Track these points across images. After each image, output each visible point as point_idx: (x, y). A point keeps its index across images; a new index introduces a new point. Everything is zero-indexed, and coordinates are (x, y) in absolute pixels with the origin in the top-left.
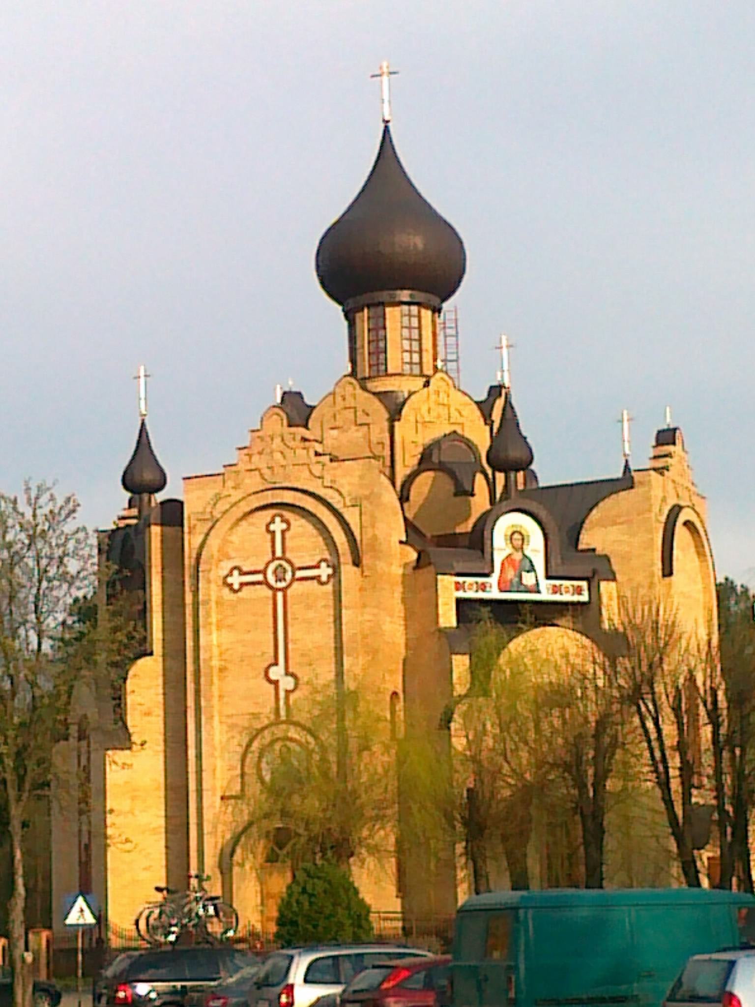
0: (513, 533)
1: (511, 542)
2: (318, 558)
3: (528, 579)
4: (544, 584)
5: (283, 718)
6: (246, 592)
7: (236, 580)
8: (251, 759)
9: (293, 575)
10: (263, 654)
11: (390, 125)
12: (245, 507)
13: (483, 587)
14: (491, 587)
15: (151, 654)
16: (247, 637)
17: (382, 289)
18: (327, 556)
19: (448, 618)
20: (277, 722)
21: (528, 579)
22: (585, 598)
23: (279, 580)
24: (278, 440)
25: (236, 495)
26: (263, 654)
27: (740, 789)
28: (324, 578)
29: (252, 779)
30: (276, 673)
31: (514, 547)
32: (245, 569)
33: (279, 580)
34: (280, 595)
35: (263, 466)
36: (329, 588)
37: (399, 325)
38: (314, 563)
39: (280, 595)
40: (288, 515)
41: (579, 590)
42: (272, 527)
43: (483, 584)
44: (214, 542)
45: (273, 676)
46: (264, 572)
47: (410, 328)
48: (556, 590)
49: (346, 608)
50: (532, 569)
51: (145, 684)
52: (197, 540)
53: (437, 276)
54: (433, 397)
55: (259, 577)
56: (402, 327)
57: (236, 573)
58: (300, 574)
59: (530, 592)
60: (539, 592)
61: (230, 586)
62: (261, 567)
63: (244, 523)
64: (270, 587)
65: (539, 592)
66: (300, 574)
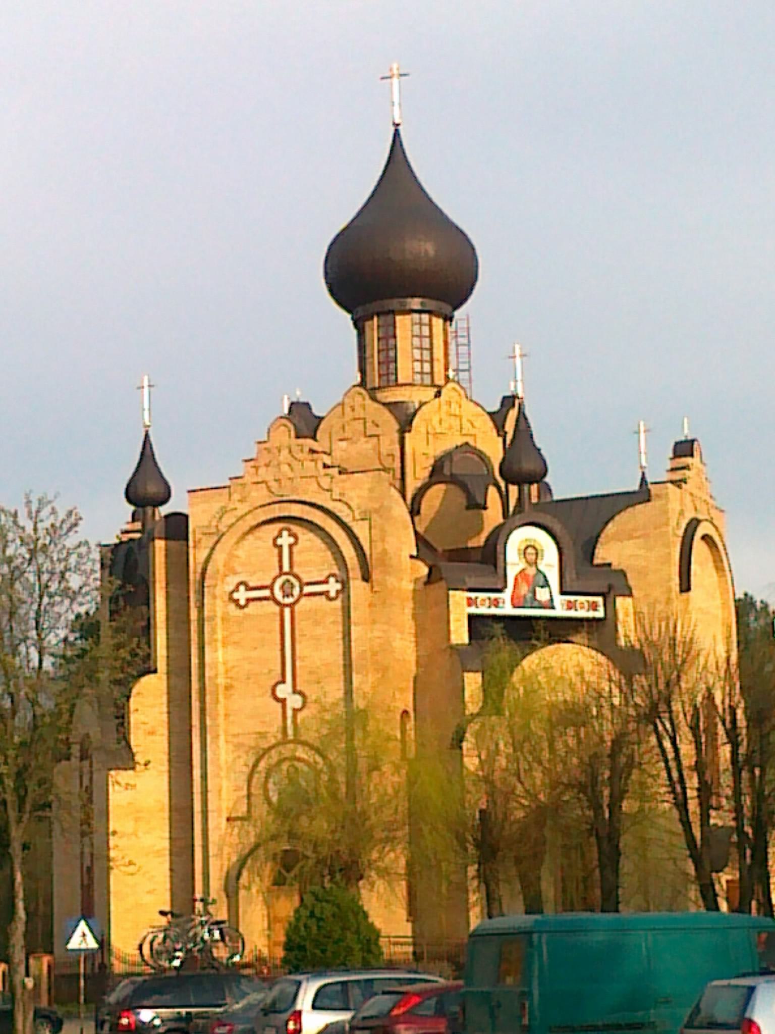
0: (527, 548)
1: (525, 557)
2: (326, 573)
3: (542, 595)
4: (559, 600)
5: (291, 737)
6: (253, 607)
7: (242, 595)
8: (258, 779)
9: (301, 590)
10: (270, 671)
11: (400, 128)
12: (251, 521)
13: (496, 603)
14: (504, 602)
15: (155, 671)
16: (254, 654)
17: (392, 297)
18: (335, 570)
19: (460, 634)
20: (284, 741)
21: (542, 595)
22: (600, 614)
23: (286, 595)
24: (285, 452)
25: (243, 509)
26: (270, 671)
27: (759, 810)
28: (333, 594)
29: (258, 800)
30: (284, 691)
31: (527, 562)
32: (252, 584)
33: (286, 595)
34: (287, 611)
35: (270, 478)
36: (338, 603)
37: (410, 333)
38: (322, 579)
39: (287, 611)
40: (295, 529)
41: (594, 606)
42: (279, 541)
43: (496, 600)
44: (219, 557)
45: (280, 695)
46: (271, 587)
47: (421, 337)
48: (570, 606)
49: (355, 624)
50: (546, 584)
51: (149, 702)
52: (203, 554)
53: (449, 284)
54: (445, 408)
55: (266, 593)
56: (413, 336)
57: (242, 588)
58: (307, 589)
59: (544, 607)
60: (553, 608)
61: (236, 601)
62: (268, 582)
63: (250, 537)
64: (278, 603)
65: (553, 608)
66: (307, 589)
